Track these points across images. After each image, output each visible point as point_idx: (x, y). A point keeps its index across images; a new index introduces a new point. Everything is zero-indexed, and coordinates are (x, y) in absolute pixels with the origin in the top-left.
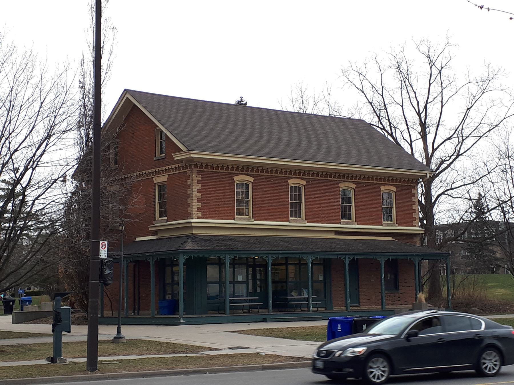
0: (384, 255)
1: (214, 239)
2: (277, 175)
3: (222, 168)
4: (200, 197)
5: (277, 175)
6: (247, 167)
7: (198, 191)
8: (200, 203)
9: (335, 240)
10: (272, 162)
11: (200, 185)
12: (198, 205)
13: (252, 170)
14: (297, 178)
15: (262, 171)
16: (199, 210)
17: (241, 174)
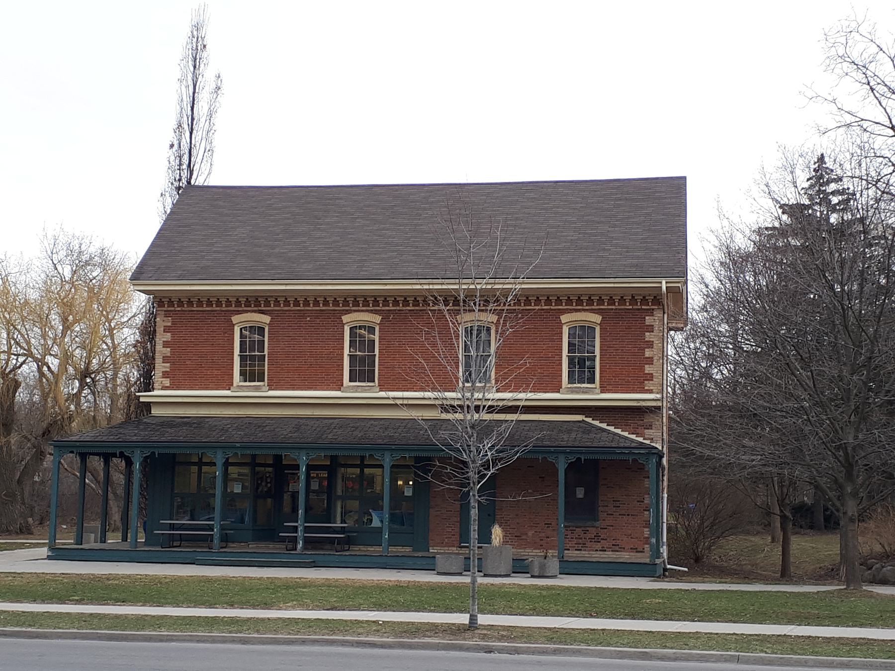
0: (564, 452)
1: (185, 422)
2: (387, 308)
3: (210, 303)
4: (169, 355)
5: (387, 308)
6: (254, 299)
7: (166, 344)
8: (168, 365)
9: (247, 421)
10: (288, 287)
11: (169, 334)
12: (165, 367)
13: (267, 304)
14: (362, 311)
15: (306, 303)
16: (165, 375)
17: (247, 311)
